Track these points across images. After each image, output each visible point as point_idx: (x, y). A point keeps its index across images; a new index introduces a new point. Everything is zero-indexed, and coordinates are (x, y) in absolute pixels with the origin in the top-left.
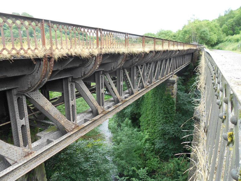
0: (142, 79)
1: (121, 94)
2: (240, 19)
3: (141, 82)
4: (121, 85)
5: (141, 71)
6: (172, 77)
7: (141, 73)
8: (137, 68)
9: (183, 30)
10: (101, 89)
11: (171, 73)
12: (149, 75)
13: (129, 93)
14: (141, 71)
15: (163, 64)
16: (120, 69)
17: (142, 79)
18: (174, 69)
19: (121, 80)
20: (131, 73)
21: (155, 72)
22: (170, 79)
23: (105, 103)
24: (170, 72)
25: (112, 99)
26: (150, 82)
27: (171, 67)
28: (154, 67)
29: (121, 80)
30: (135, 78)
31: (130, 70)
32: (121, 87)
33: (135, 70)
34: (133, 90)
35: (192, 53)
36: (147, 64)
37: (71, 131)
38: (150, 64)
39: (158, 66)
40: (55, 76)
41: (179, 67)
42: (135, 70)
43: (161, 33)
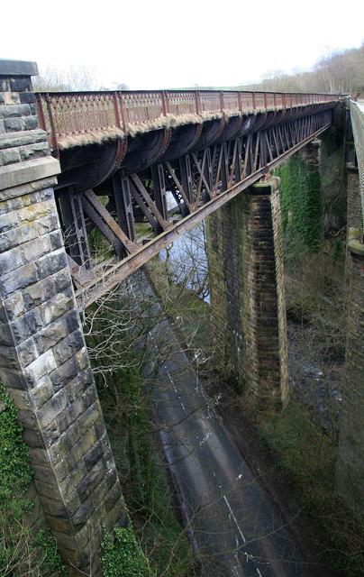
0: (205, 182)
1: (132, 233)
2: (227, 575)
7: (202, 172)
8: (191, 158)
16: (156, 164)
17: (205, 182)
18: (269, 157)
22: (258, 185)
23: (136, 235)
24: (257, 169)
25: (149, 225)
26: (224, 188)
27: (259, 156)
30: (190, 179)
31: (175, 164)
32: (130, 218)
33: (188, 163)
35: (333, 110)
36: (212, 149)
38: (219, 147)
41: (281, 152)
42: (188, 163)
43: (266, 83)
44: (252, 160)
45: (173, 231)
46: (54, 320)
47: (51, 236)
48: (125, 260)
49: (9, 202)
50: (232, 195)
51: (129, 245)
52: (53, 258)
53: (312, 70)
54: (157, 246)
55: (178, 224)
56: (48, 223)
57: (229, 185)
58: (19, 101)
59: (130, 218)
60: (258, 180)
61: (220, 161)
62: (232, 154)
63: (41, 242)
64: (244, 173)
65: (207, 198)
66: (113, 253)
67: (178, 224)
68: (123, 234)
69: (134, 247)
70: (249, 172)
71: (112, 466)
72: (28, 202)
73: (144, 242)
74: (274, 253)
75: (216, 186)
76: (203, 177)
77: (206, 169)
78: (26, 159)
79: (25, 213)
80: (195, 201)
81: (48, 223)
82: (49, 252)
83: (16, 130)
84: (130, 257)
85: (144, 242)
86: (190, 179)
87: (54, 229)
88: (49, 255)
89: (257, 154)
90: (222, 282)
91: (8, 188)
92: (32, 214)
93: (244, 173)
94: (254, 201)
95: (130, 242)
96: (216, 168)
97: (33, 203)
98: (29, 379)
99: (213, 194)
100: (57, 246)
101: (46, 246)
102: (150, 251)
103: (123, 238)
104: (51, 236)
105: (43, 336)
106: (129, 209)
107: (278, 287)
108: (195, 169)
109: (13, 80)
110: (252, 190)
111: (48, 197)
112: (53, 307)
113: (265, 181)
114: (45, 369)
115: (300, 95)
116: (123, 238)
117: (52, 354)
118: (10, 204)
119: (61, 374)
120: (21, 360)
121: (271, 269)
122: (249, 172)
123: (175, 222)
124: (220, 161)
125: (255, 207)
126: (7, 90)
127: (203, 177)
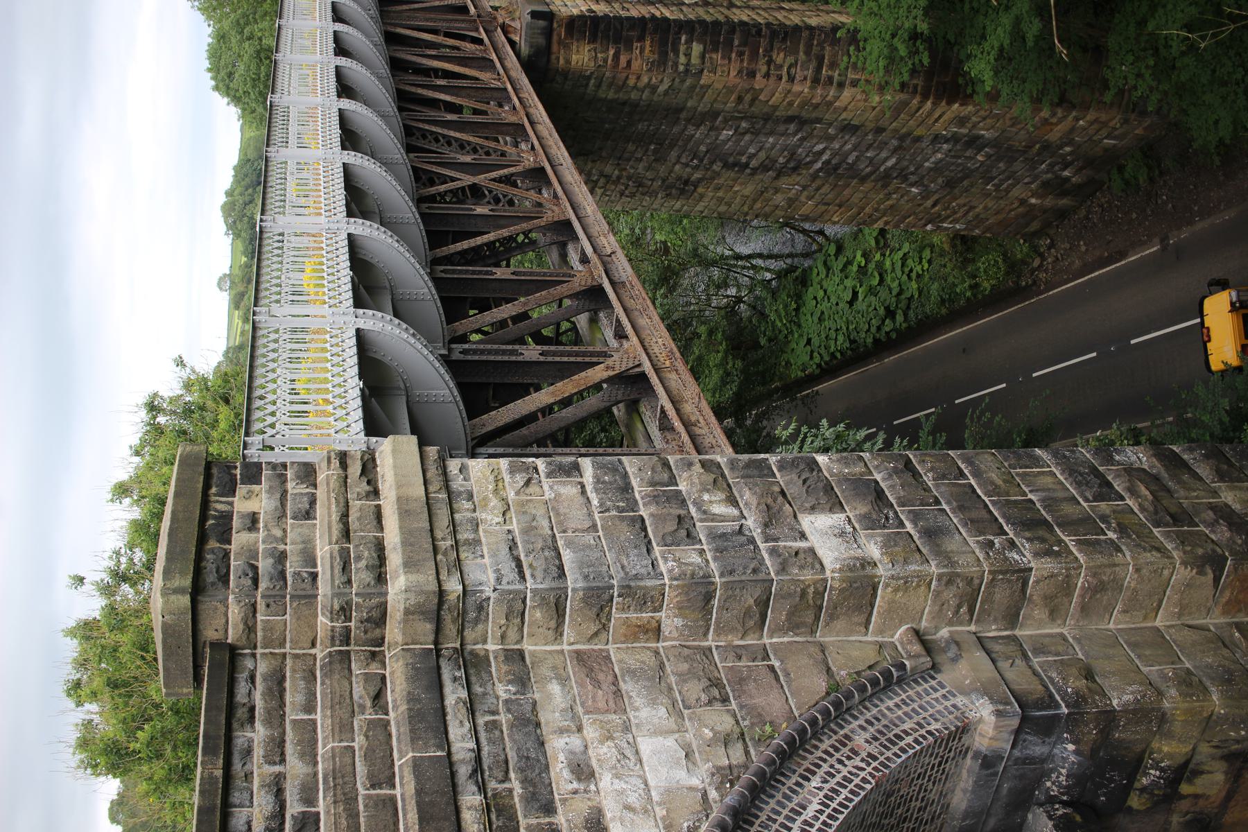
0: (494, 174)
1: (592, 354)
3: (508, 180)
4: (542, 359)
5: (453, 179)
6: (505, 29)
7: (467, 180)
9: (222, 63)
10: (520, 358)
11: (484, 36)
12: (486, 143)
13: (563, 246)
14: (453, 179)
15: (414, 59)
17: (494, 174)
19: (487, 273)
20: (497, 386)
21: (448, 74)
22: (525, 50)
24: (479, 41)
26: (517, 132)
27: (447, 35)
28: (420, 79)
29: (487, 273)
32: (554, 354)
34: (542, 222)
37: (648, 648)
39: (420, 91)
40: (387, 416)
44: (455, 53)
45: (604, 264)
46: (732, 501)
47: (549, 475)
48: (654, 380)
49: (459, 537)
50: (540, 112)
51: (618, 363)
52: (598, 480)
53: (270, 807)
54: (631, 304)
55: (589, 250)
56: (520, 479)
57: (512, 119)
58: (256, 487)
59: (554, 354)
60: (512, 44)
61: (446, 132)
62: (434, 104)
63: (558, 495)
64: (485, 76)
65: (538, 176)
66: (633, 407)
67: (589, 250)
68: (590, 372)
69: (625, 355)
70: (486, 64)
71: (1139, 456)
72: (467, 505)
73: (620, 335)
74: (716, 23)
75: (509, 149)
76: (480, 179)
77: (463, 167)
78: (376, 493)
79: (490, 517)
80: (540, 205)
81: (520, 479)
82: (583, 487)
83: (313, 502)
84: (647, 367)
85: (620, 335)
86: (480, 210)
87: (536, 469)
88: (589, 488)
89: (440, 39)
90: (784, 183)
91: (432, 531)
92: (494, 502)
93: (485, 76)
94: (568, 62)
95: (609, 362)
96: (462, 146)
97: (470, 497)
98: (851, 569)
99: (529, 161)
100: (576, 467)
101: (569, 490)
102: (642, 322)
103: (597, 374)
104: (549, 475)
105: (766, 525)
106: (531, 352)
107: (813, 22)
108: (460, 195)
109: (214, 490)
110: (539, 68)
111: (462, 469)
112: (706, 497)
113: (517, 24)
114: (842, 534)
115: (255, 183)
116: (597, 374)
117: (811, 518)
118: (464, 535)
119: (863, 509)
120: (808, 576)
121: (759, 32)
122: (486, 64)
123: (584, 260)
124: (446, 132)
125: (581, 57)
126: (231, 504)
127: (480, 179)
